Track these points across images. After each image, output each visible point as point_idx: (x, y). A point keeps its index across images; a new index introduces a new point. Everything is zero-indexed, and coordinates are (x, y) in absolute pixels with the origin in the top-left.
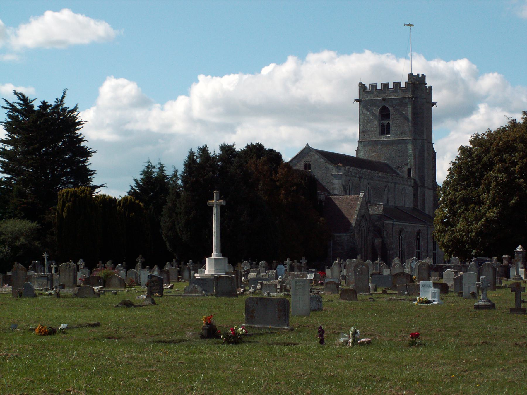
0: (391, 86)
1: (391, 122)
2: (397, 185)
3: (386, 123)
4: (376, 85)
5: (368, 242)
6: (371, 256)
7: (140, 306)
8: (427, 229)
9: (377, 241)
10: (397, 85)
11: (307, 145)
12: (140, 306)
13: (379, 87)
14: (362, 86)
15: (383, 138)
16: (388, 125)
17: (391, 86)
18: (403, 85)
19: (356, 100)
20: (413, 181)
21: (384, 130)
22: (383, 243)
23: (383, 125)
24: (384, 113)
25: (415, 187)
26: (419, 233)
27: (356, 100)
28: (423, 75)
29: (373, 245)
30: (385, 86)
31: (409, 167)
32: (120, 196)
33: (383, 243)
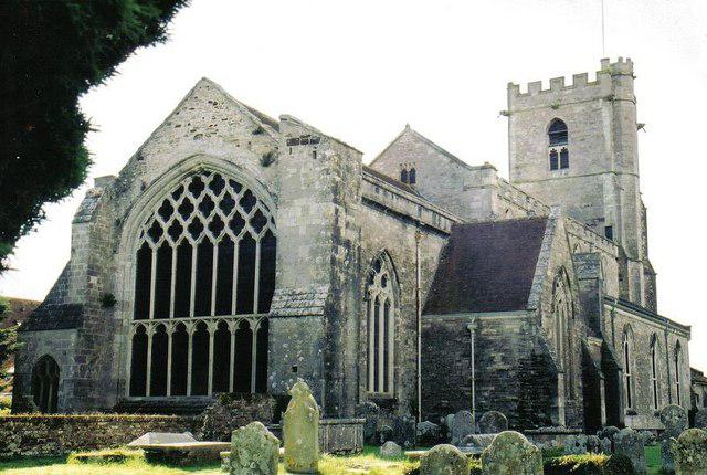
0: (569, 82)
1: (569, 147)
2: (580, 277)
3: (558, 149)
4: (540, 83)
5: (574, 345)
6: (581, 384)
7: (285, 317)
8: (666, 335)
9: (593, 344)
10: (580, 78)
11: (408, 126)
12: (285, 317)
13: (546, 86)
14: (512, 87)
15: (555, 174)
16: (565, 153)
17: (569, 82)
18: (592, 78)
19: (505, 114)
20: (617, 248)
21: (559, 161)
22: (605, 351)
23: (554, 154)
24: (558, 131)
25: (622, 259)
26: (654, 337)
27: (505, 114)
28: (628, 60)
29: (585, 354)
30: (558, 82)
31: (607, 224)
32: (36, 230)
33: (605, 351)
